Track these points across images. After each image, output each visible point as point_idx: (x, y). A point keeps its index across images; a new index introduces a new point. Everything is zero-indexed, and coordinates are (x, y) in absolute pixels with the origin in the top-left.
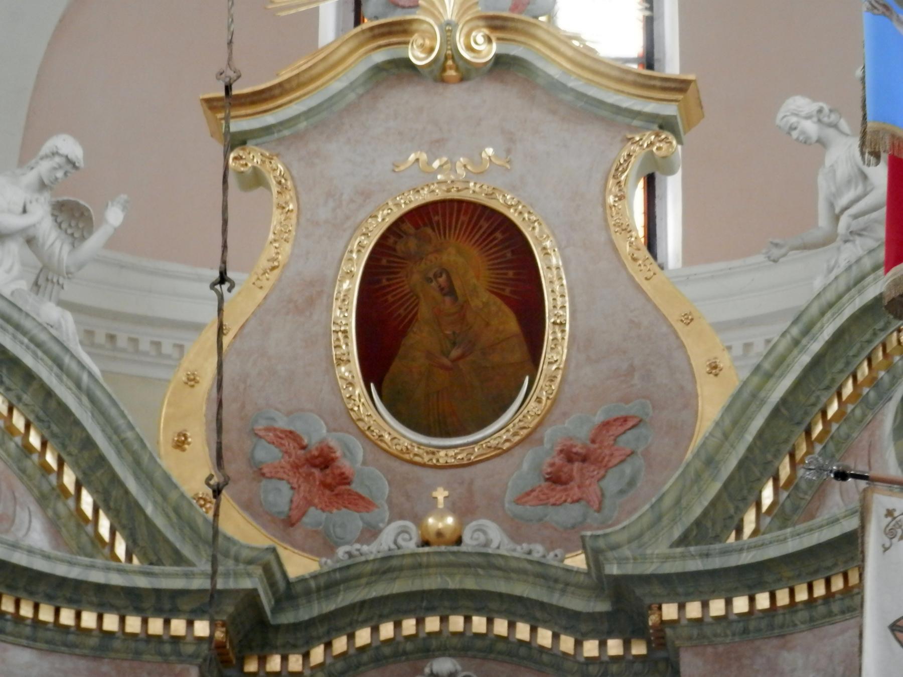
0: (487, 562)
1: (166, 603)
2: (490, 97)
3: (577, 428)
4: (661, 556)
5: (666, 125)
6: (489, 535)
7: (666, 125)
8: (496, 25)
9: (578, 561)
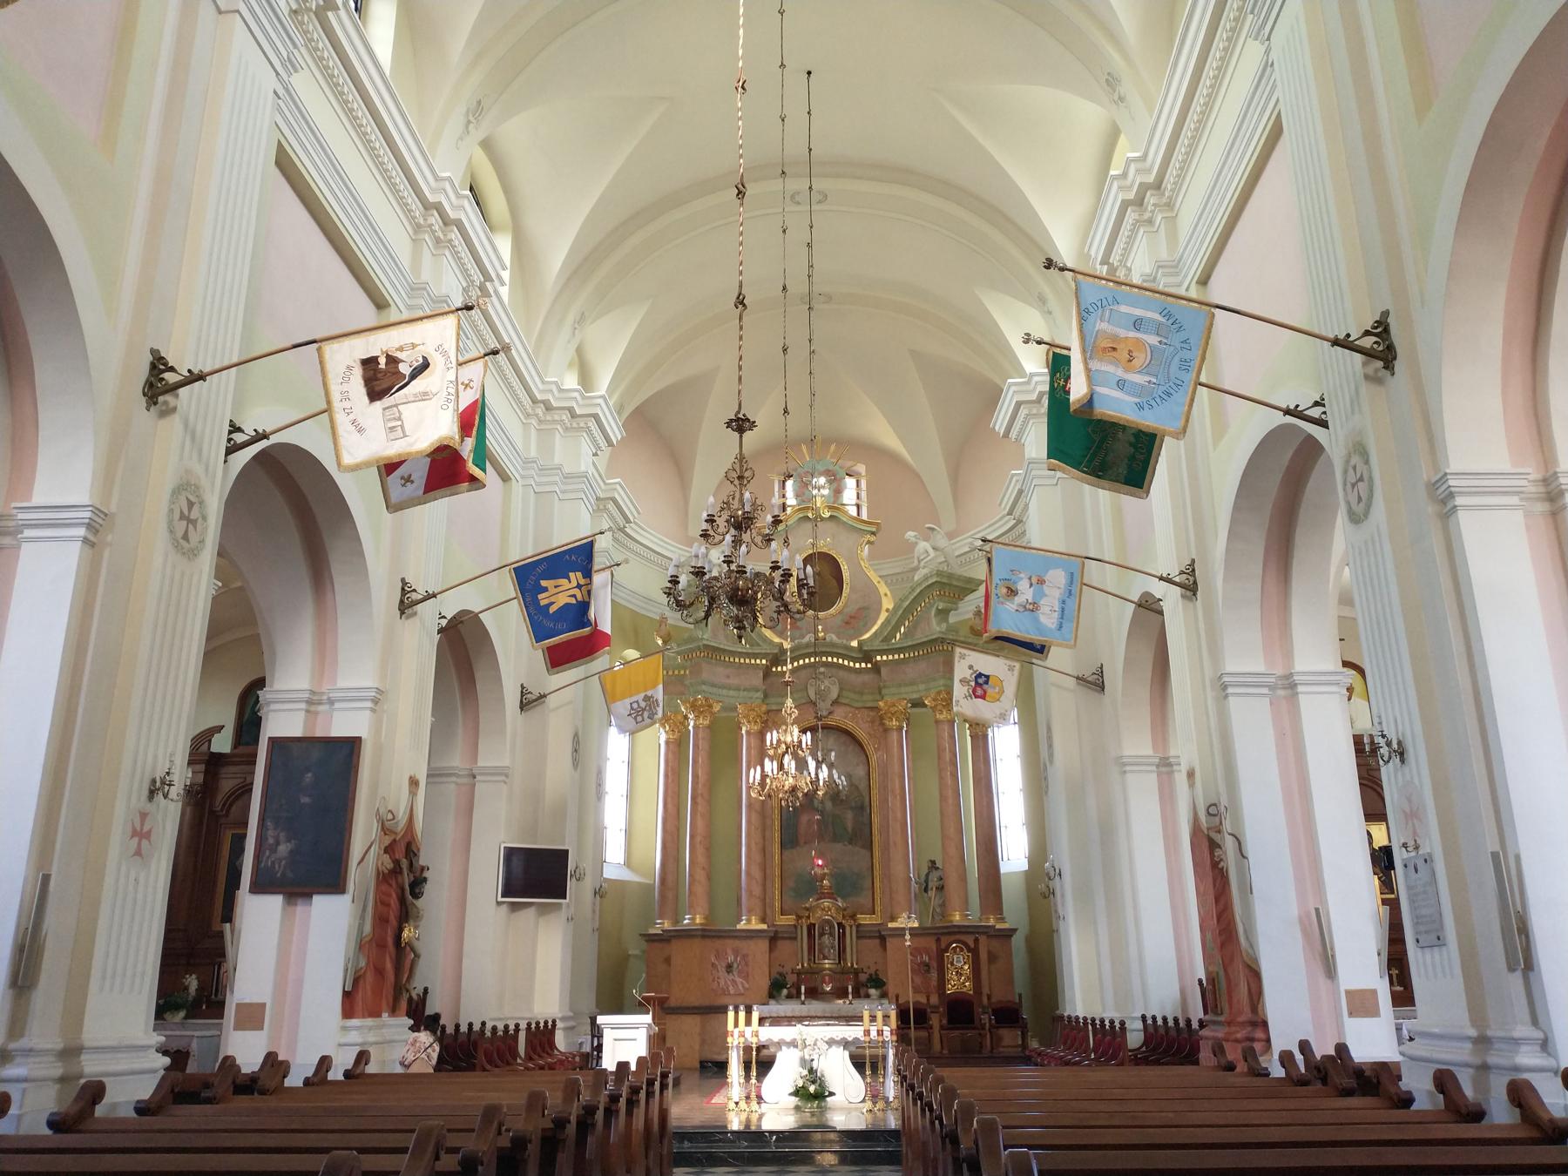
0: (833, 645)
1: (756, 656)
2: (830, 525)
3: (852, 609)
4: (877, 645)
5: (873, 533)
6: (832, 637)
7: (873, 533)
8: (830, 508)
9: (854, 644)
